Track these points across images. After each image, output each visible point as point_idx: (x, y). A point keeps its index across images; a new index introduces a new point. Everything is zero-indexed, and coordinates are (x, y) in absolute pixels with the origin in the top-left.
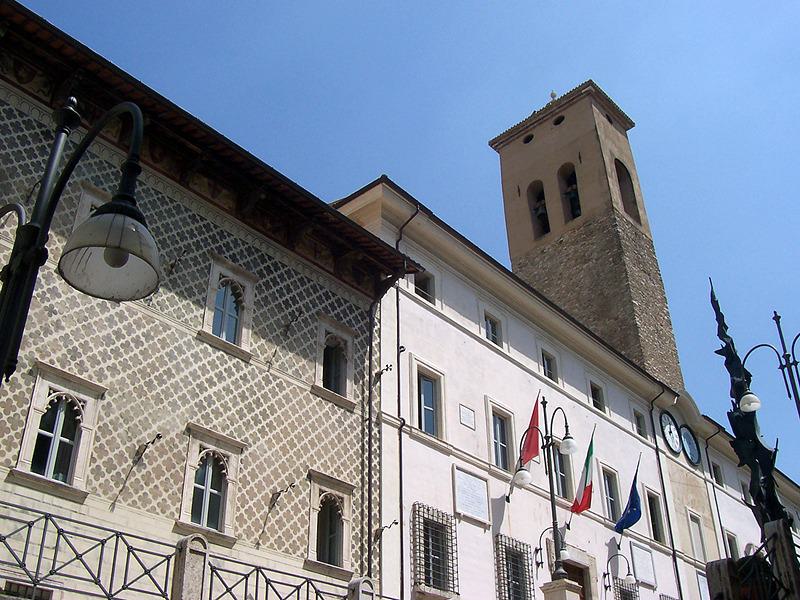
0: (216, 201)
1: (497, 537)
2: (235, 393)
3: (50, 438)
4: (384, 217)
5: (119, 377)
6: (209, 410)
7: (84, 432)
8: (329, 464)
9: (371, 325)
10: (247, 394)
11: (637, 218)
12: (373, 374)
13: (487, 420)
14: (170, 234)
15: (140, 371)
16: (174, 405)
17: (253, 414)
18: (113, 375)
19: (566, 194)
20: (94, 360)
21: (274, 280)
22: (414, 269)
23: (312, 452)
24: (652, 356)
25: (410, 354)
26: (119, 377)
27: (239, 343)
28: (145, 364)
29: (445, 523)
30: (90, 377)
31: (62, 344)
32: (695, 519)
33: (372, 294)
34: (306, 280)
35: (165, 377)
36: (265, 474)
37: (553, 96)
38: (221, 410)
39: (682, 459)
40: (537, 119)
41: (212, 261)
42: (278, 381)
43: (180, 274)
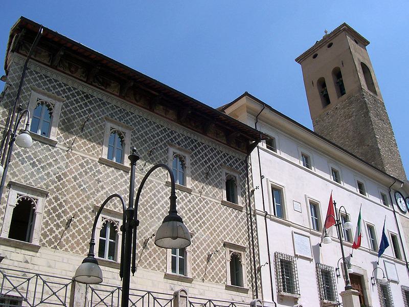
0: (168, 116)
2: (186, 209)
3: (105, 241)
9: (247, 167)
10: (192, 209)
11: (375, 92)
17: (195, 218)
23: (225, 233)
24: (387, 163)
27: (186, 185)
30: (119, 210)
33: (246, 152)
34: (214, 149)
35: (153, 206)
36: (203, 247)
37: (326, 32)
40: (319, 45)
41: (169, 146)
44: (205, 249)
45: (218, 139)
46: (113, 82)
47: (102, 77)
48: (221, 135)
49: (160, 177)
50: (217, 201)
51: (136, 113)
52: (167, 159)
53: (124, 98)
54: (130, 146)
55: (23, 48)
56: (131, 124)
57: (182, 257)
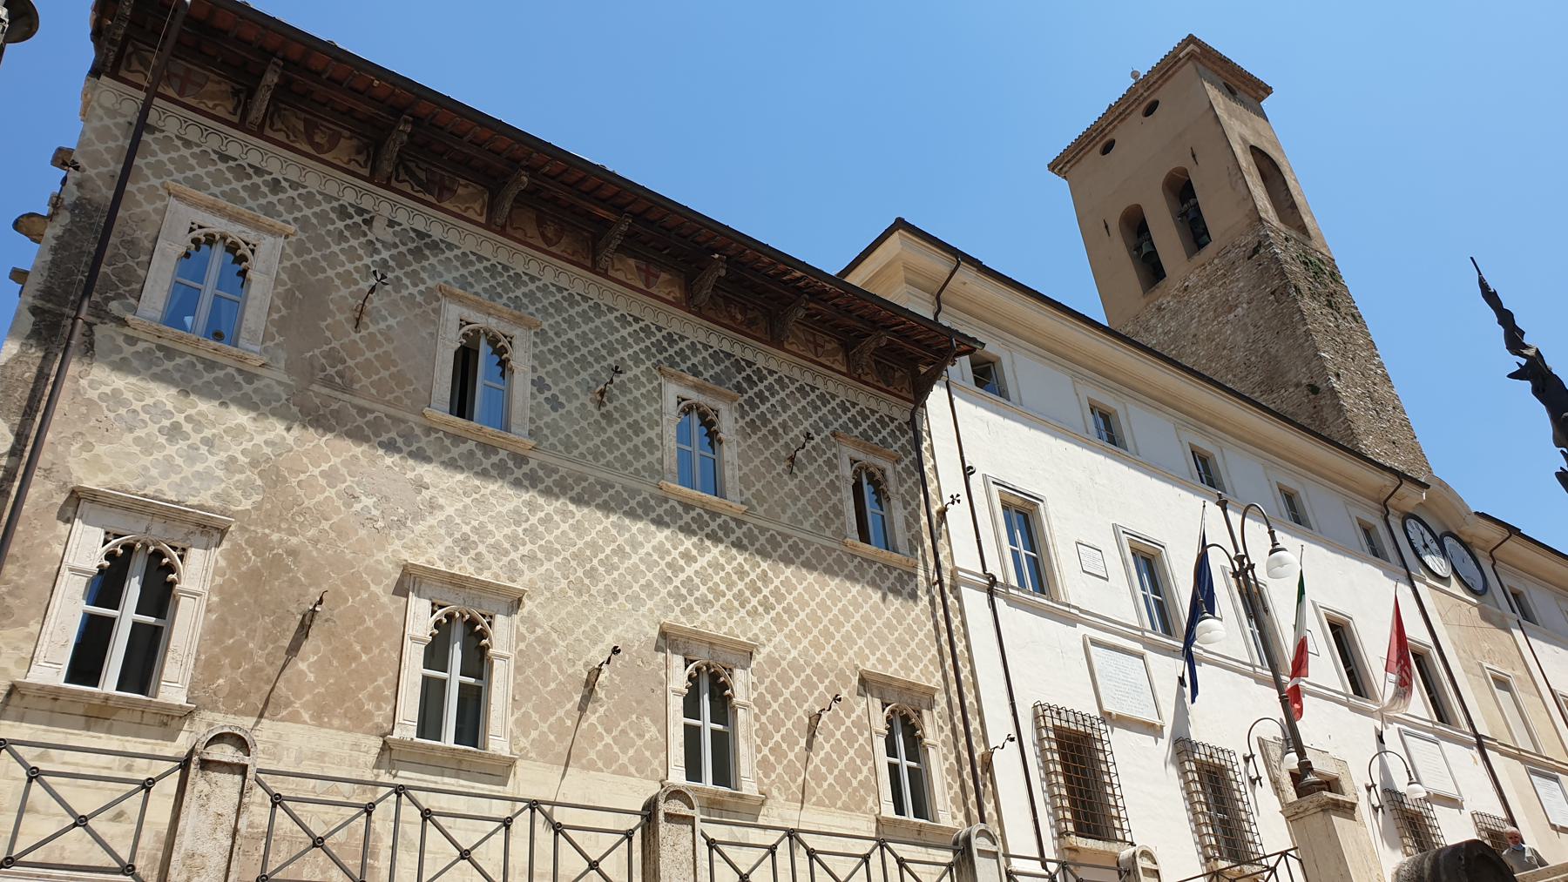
0: (653, 290)
1: (1183, 747)
2: (728, 568)
4: (908, 282)
5: (542, 570)
6: (691, 600)
7: (497, 663)
8: (889, 658)
9: (917, 441)
11: (1303, 229)
12: (934, 512)
13: (1125, 562)
14: (591, 347)
15: (575, 556)
16: (634, 599)
18: (532, 568)
19: (1181, 215)
20: (496, 548)
21: (760, 395)
22: (969, 346)
23: (861, 643)
24: (1367, 433)
25: (985, 476)
26: (542, 570)
28: (580, 544)
29: (1089, 731)
31: (443, 532)
32: (1502, 683)
33: (911, 397)
35: (616, 559)
36: (792, 688)
38: (710, 597)
39: (1455, 588)
40: (1118, 113)
42: (790, 542)
43: (616, 403)
44: (799, 697)
45: (822, 360)
46: (462, 182)
47: (424, 166)
48: (829, 347)
49: (637, 471)
50: (827, 543)
51: (548, 277)
52: (657, 417)
53: (502, 231)
54: (530, 376)
55: (136, 65)
56: (532, 309)
57: (720, 727)
